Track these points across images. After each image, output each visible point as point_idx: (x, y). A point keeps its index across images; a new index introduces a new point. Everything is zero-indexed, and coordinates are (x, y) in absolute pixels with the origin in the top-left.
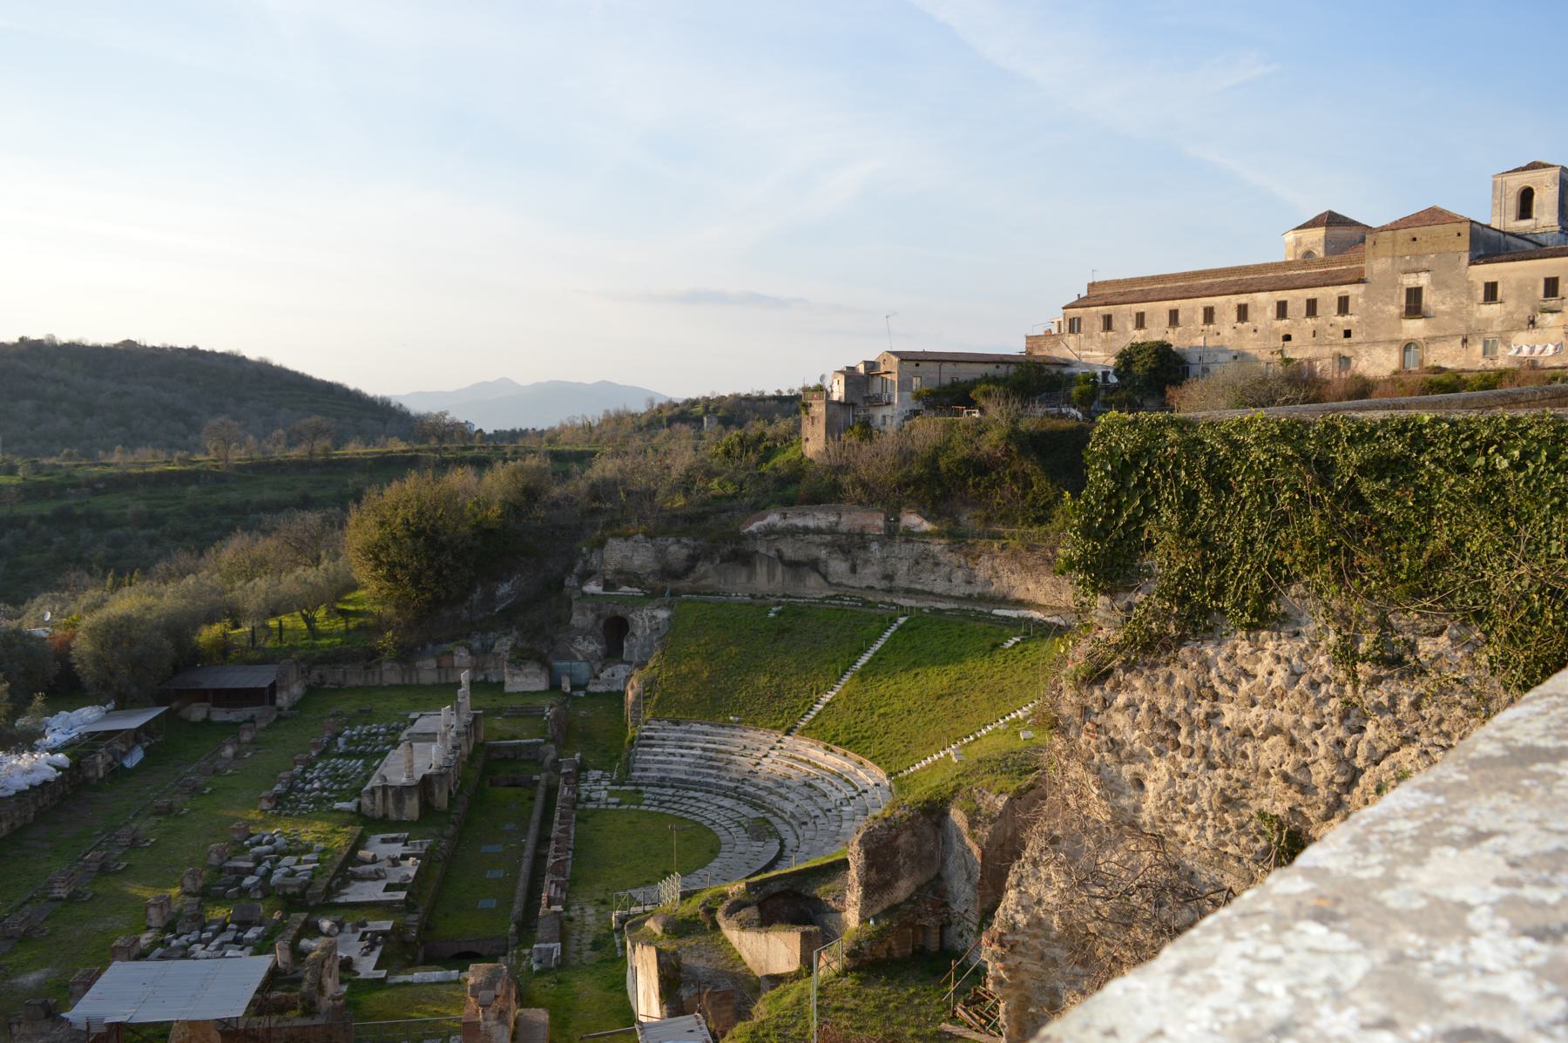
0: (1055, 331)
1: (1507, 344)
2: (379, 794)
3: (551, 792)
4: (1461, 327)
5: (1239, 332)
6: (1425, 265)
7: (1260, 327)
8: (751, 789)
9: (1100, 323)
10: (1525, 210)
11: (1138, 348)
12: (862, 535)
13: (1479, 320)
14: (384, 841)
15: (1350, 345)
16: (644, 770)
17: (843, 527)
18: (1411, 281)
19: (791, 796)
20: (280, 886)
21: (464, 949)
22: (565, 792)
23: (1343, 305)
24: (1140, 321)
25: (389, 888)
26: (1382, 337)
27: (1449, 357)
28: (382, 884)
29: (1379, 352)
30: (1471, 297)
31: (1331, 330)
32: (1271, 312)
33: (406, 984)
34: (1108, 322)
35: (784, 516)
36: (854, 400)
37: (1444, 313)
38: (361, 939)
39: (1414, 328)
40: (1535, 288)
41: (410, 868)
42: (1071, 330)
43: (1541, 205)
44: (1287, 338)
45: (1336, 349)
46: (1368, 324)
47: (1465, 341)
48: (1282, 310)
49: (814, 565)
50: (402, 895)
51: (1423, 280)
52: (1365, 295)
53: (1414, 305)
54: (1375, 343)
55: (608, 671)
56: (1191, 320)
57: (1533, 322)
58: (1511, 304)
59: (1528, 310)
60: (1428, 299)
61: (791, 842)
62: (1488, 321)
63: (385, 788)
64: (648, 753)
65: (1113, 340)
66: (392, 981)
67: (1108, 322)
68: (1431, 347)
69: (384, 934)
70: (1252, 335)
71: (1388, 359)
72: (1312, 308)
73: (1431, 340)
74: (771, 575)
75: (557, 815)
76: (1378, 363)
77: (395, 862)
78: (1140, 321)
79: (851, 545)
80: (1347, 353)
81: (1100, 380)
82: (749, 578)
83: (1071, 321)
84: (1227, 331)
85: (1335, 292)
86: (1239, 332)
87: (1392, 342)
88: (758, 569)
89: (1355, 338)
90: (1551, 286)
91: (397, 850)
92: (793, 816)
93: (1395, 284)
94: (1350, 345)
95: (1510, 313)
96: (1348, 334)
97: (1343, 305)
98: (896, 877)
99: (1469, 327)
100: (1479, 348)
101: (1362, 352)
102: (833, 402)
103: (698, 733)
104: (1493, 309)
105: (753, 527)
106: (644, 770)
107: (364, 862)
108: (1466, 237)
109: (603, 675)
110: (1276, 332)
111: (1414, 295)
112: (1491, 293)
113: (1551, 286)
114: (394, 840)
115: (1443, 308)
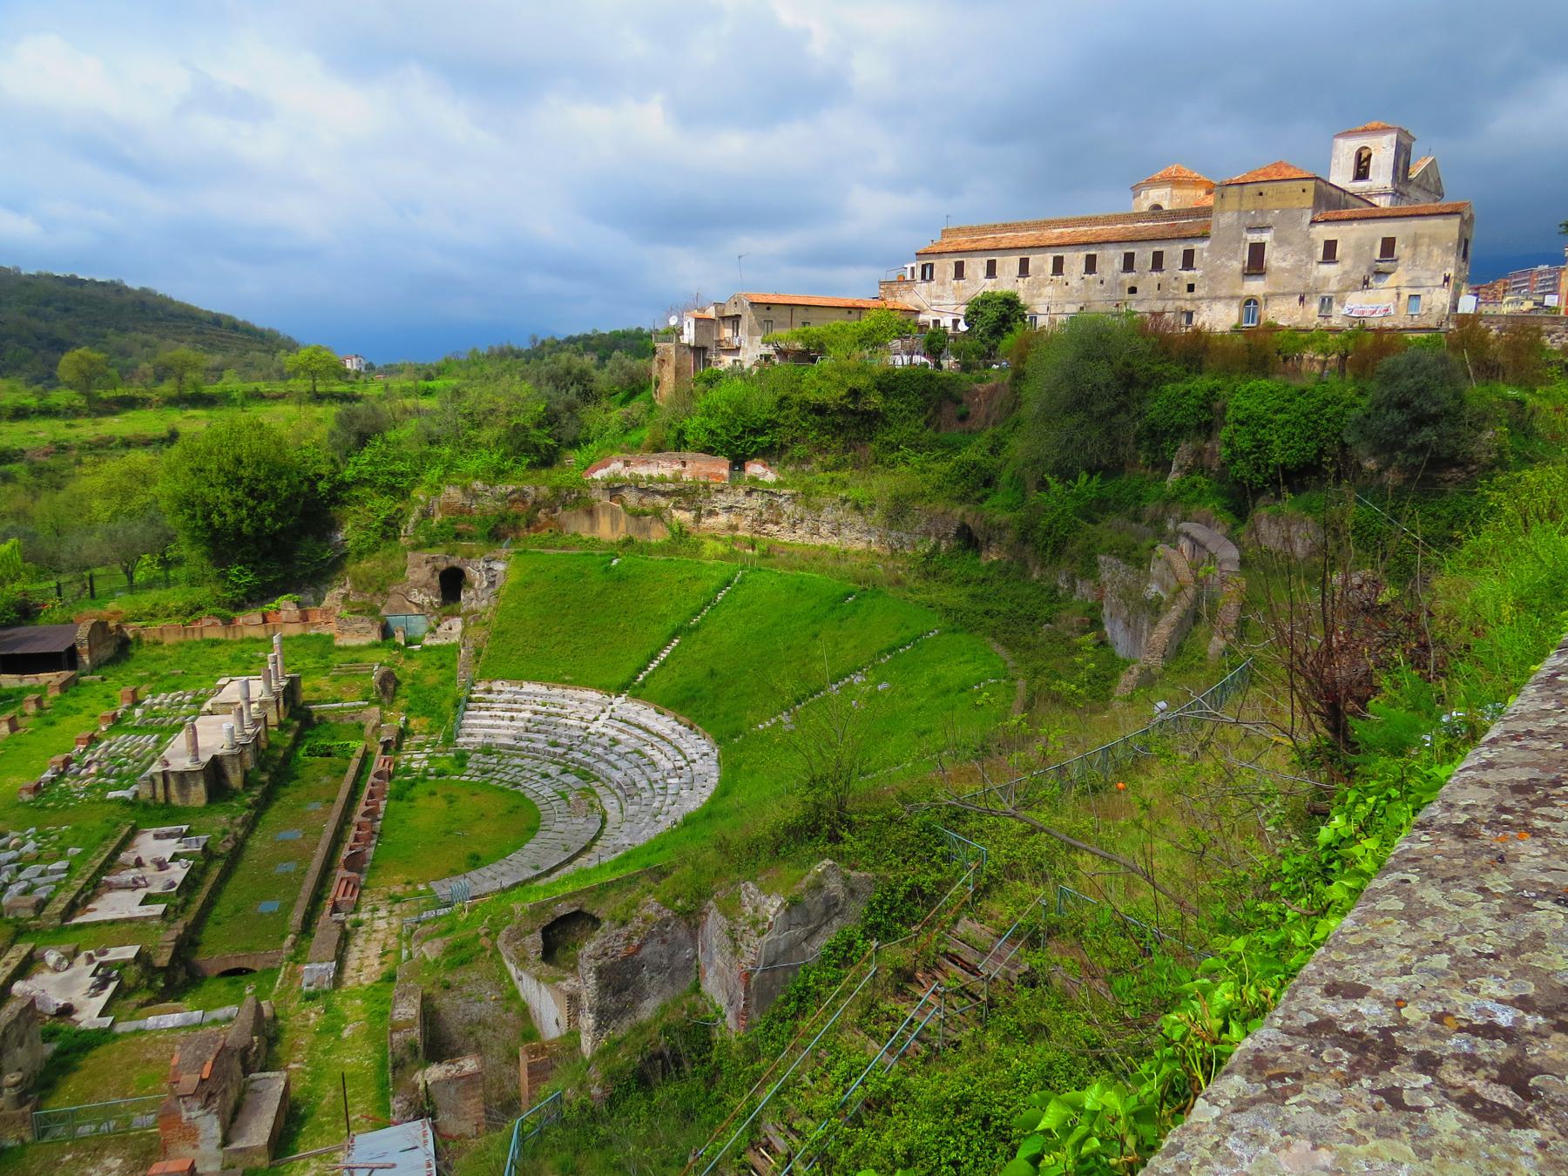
0: (909, 277)
1: (1342, 303)
2: (160, 781)
3: (366, 757)
4: (1299, 286)
5: (1087, 283)
6: (1269, 220)
7: (1107, 278)
8: (579, 756)
9: (952, 271)
10: (1362, 172)
11: (986, 301)
12: (706, 486)
13: (1316, 279)
14: (157, 837)
15: (1192, 300)
16: (469, 735)
17: (687, 476)
18: (1254, 238)
19: (620, 764)
20: (11, 909)
21: (233, 966)
22: (378, 763)
23: (1188, 260)
24: (991, 270)
25: (148, 900)
26: (1223, 292)
27: (1283, 313)
28: (140, 894)
29: (1219, 307)
30: (1311, 255)
31: (1175, 284)
32: (1118, 263)
33: (140, 1031)
34: (959, 272)
35: (627, 464)
36: (704, 343)
37: (1284, 270)
38: (94, 974)
39: (1255, 287)
40: (1372, 248)
41: (178, 872)
42: (923, 277)
43: (1378, 166)
44: (1133, 290)
45: (1178, 303)
46: (1211, 279)
47: (1302, 299)
48: (1129, 263)
49: (658, 513)
50: (159, 909)
51: (1266, 237)
52: (1209, 250)
53: (1256, 264)
54: (1217, 298)
55: (446, 625)
56: (1040, 270)
57: (1366, 282)
58: (1347, 264)
59: (1363, 270)
60: (1272, 257)
61: (613, 815)
62: (1326, 280)
63: (165, 775)
64: (475, 717)
65: (964, 287)
66: (120, 1028)
67: (959, 272)
68: (1270, 303)
69: (125, 964)
70: (1098, 287)
71: (1228, 315)
72: (1158, 262)
73: (1267, 297)
74: (614, 524)
75: (365, 793)
76: (1219, 317)
77: (161, 865)
78: (991, 270)
79: (687, 495)
80: (1189, 307)
81: (950, 330)
82: (592, 527)
83: (924, 267)
84: (1075, 282)
85: (1180, 248)
86: (1087, 283)
87: (1233, 298)
88: (602, 519)
89: (1198, 292)
90: (1388, 246)
91: (169, 847)
92: (619, 786)
93: (1240, 240)
94: (1192, 300)
95: (1346, 273)
96: (1191, 288)
97: (1188, 260)
98: (640, 995)
99: (1307, 285)
100: (1316, 306)
101: (1204, 307)
102: (684, 346)
103: (529, 694)
104: (1327, 269)
105: (598, 475)
106: (469, 735)
107: (126, 866)
108: (1311, 194)
109: (440, 630)
110: (1121, 284)
111: (1257, 250)
112: (1330, 247)
113: (1388, 246)
114: (169, 836)
115: (1284, 265)
